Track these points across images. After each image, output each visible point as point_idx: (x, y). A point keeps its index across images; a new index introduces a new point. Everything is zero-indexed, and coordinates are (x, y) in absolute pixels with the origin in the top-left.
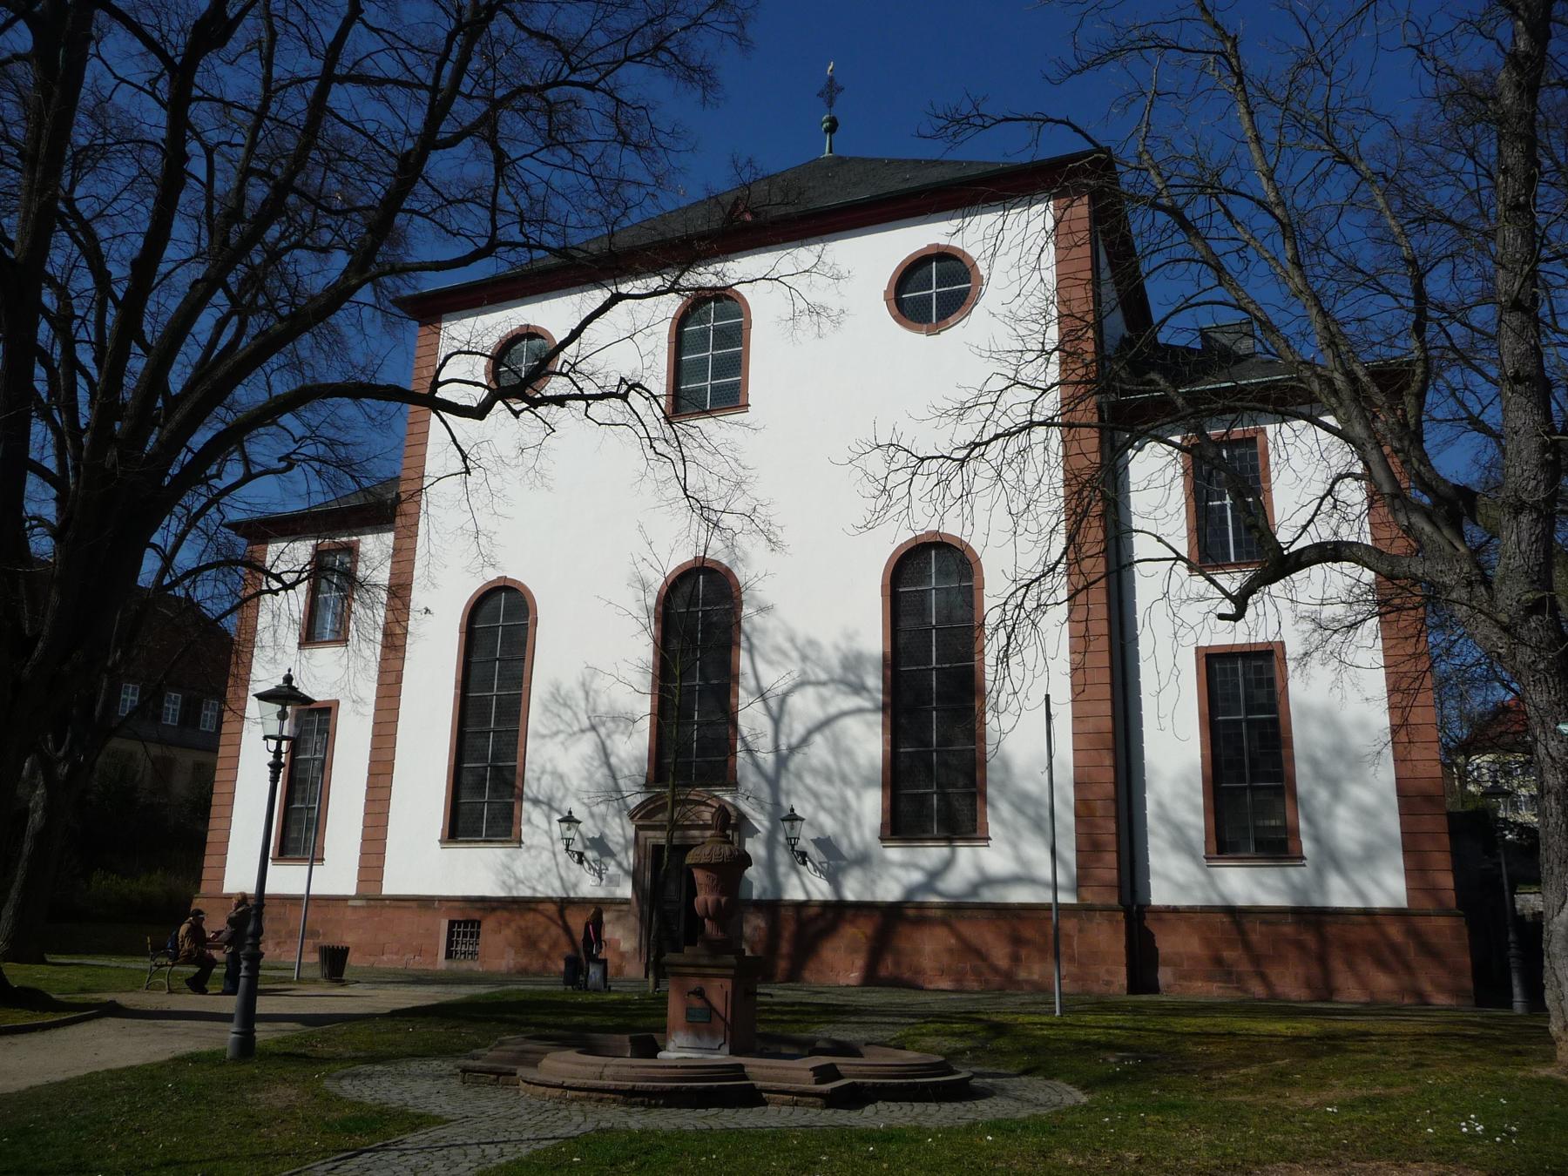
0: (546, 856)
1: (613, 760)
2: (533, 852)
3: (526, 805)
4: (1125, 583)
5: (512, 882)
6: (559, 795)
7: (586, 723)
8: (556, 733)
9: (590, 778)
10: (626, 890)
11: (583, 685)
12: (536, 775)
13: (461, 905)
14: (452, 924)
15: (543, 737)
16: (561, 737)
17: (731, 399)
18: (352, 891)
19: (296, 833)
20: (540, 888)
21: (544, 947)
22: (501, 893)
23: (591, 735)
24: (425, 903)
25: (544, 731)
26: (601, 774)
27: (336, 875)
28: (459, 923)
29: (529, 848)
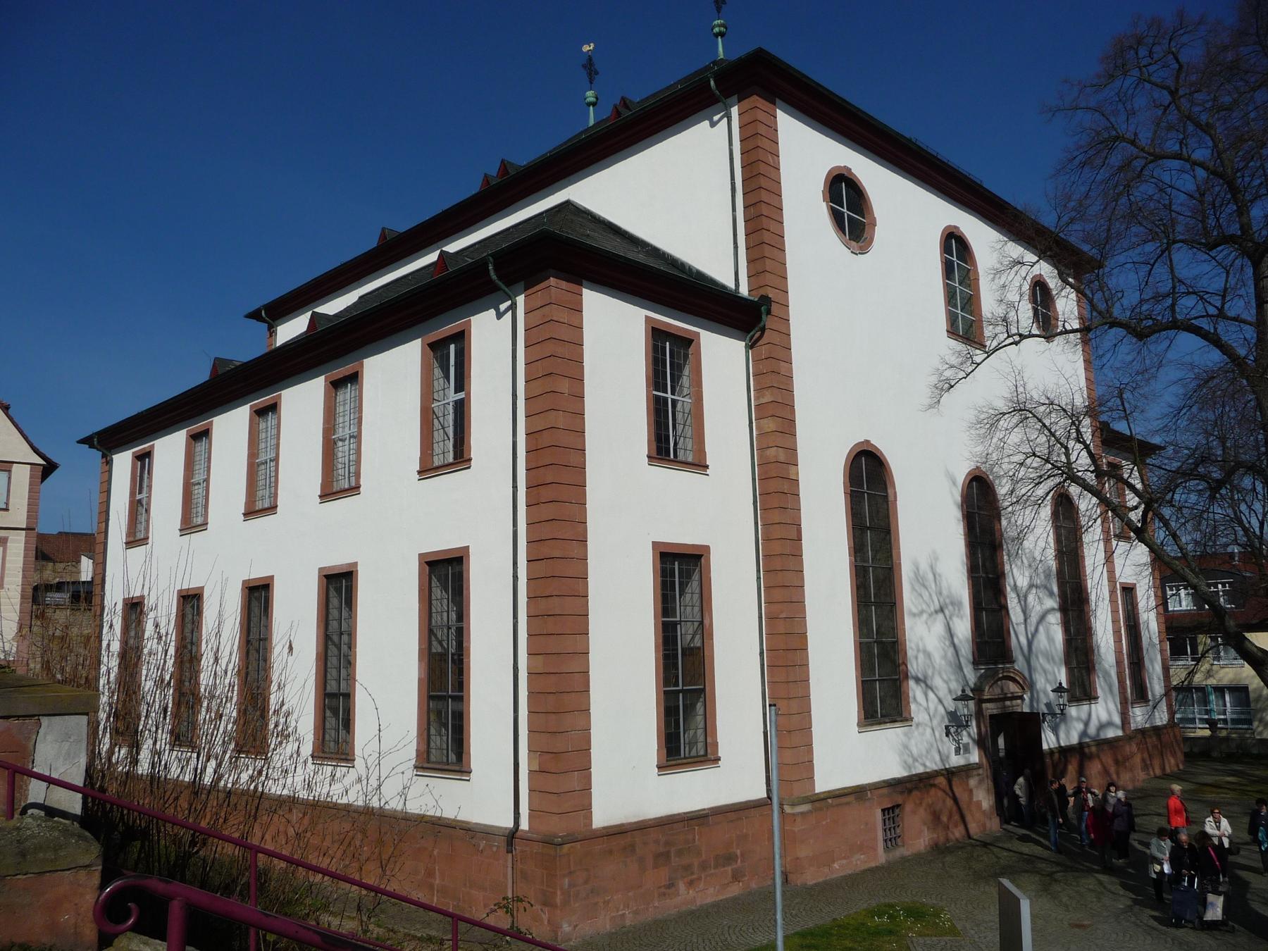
0: (929, 731)
1: (956, 641)
2: (921, 729)
3: (912, 683)
4: (322, 630)
5: (910, 761)
6: (930, 673)
7: (937, 607)
8: (922, 612)
9: (945, 657)
10: (975, 757)
11: (932, 567)
12: (915, 653)
13: (885, 791)
14: (883, 810)
15: (914, 615)
16: (925, 616)
17: (144, 541)
18: (758, 792)
19: (684, 730)
20: (928, 764)
21: (944, 819)
22: (905, 774)
23: (941, 616)
24: (859, 792)
25: (914, 610)
26: (950, 651)
27: (737, 773)
28: (888, 809)
29: (918, 725)
